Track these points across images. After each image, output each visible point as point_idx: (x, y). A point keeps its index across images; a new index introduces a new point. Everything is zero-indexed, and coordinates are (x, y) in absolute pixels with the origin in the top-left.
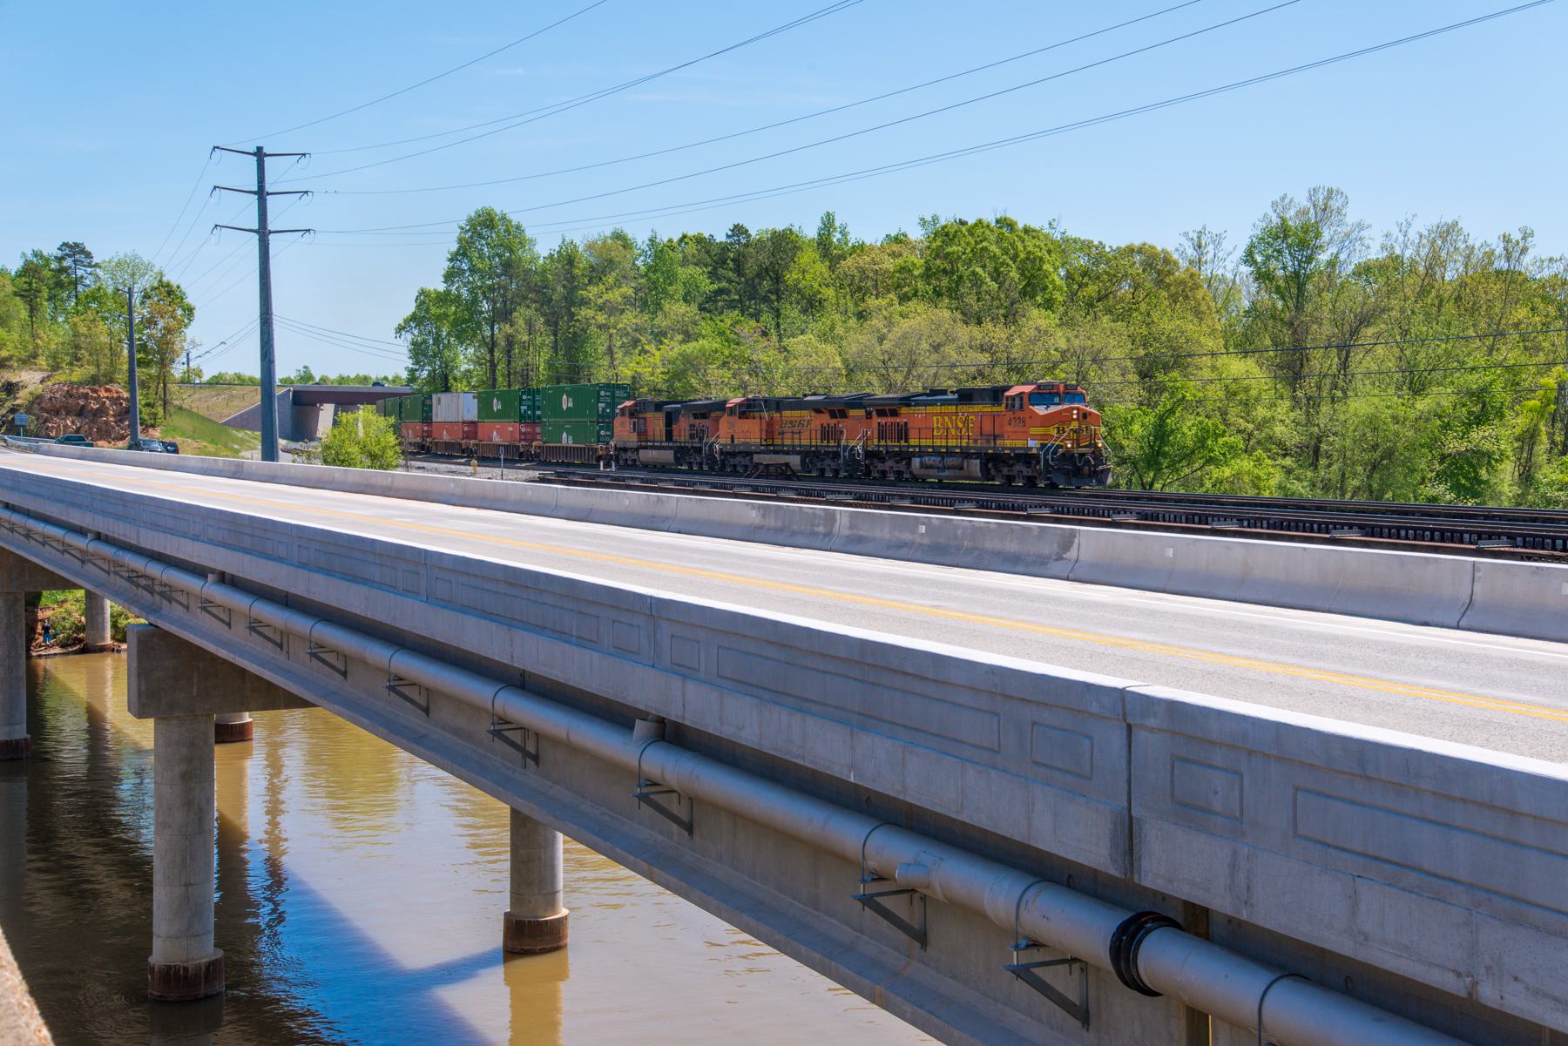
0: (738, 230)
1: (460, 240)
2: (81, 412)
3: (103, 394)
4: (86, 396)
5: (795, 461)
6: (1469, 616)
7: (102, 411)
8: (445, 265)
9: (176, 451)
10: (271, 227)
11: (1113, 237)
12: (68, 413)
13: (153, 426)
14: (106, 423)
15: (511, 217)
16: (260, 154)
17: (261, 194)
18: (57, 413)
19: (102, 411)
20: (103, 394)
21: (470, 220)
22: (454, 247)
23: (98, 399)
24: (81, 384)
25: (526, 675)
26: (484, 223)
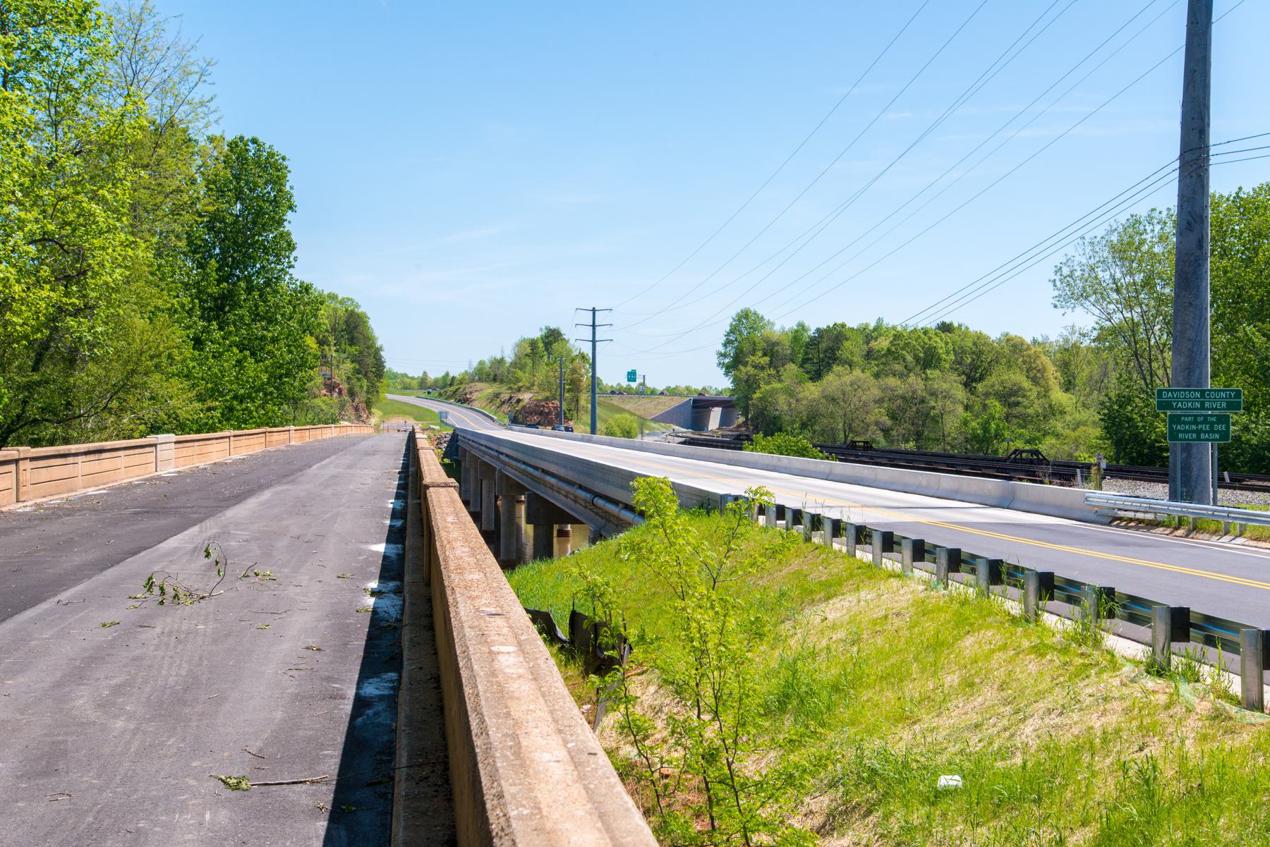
0: (618, 384)
1: (731, 325)
2: (541, 413)
3: (551, 405)
4: (543, 406)
5: (1180, 435)
6: (828, 477)
7: (550, 413)
8: (723, 339)
9: (572, 431)
10: (597, 339)
11: (994, 333)
12: (536, 414)
13: (571, 420)
14: (552, 418)
15: (758, 312)
16: (594, 310)
17: (594, 326)
18: (531, 414)
19: (550, 413)
20: (551, 405)
21: (738, 315)
22: (728, 330)
23: (548, 407)
24: (542, 401)
25: (350, 412)
26: (745, 316)
